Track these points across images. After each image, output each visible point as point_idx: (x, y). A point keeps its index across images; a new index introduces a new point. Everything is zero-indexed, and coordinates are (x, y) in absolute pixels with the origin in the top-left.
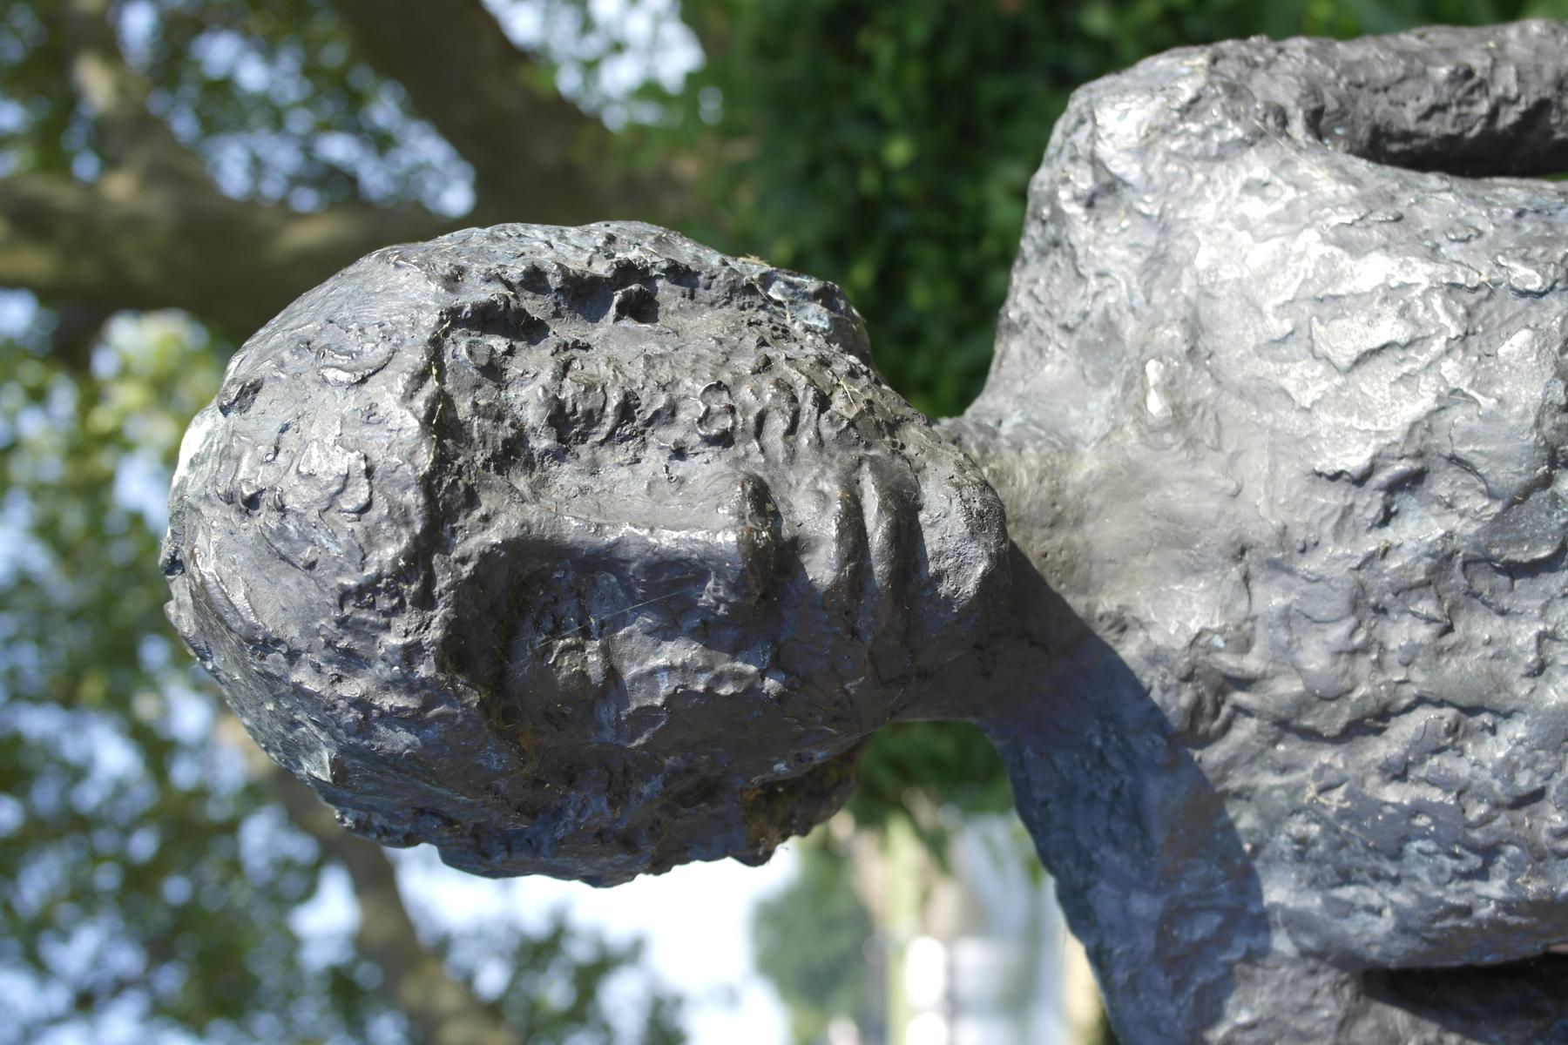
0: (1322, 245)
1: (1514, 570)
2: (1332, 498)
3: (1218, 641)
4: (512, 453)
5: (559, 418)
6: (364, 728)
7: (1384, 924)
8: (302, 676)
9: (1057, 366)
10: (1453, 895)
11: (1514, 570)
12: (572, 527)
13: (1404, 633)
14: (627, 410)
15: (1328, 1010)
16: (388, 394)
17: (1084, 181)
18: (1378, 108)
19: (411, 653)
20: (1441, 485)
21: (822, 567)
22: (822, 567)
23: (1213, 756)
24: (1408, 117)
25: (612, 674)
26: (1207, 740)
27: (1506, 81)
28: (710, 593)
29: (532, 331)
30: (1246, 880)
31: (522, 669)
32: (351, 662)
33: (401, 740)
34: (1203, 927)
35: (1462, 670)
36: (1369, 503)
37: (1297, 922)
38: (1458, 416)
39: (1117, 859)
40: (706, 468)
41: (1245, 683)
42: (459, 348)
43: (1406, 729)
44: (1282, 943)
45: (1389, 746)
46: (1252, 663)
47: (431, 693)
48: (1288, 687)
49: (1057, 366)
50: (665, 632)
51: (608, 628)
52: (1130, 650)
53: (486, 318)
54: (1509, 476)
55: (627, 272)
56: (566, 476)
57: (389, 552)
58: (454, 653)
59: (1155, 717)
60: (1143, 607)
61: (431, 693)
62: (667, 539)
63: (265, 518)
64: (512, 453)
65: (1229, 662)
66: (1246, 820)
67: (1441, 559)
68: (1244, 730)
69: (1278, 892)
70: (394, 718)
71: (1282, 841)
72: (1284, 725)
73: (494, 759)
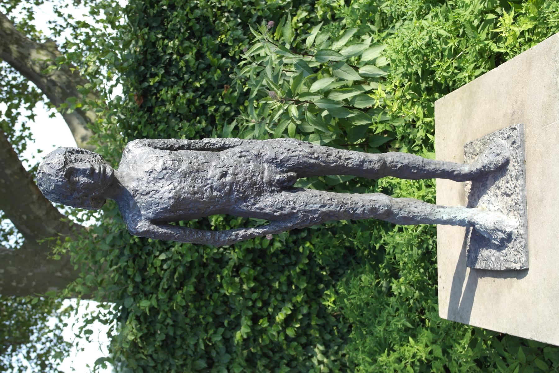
0: (33, 24)
5: (75, 159)
6: (57, 182)
7: (151, 214)
9: (124, 166)
10: (156, 209)
12: (76, 167)
13: (152, 185)
14: (81, 159)
17: (127, 150)
20: (154, 172)
21: (97, 171)
22: (97, 171)
23: (135, 198)
24: (159, 146)
25: (79, 180)
26: (135, 197)
28: (87, 172)
29: (73, 154)
30: (139, 211)
31: (71, 179)
32: (57, 176)
33: (60, 183)
34: (136, 217)
35: (155, 188)
36: (148, 174)
38: (156, 166)
40: (88, 164)
41: (138, 190)
42: (67, 153)
43: (151, 193)
44: (143, 218)
45: (150, 195)
46: (138, 189)
47: (64, 179)
48: (141, 190)
49: (124, 166)
50: (83, 177)
51: (78, 176)
52: (128, 189)
53: (69, 152)
54: (159, 171)
55: (81, 151)
56: (76, 164)
57: (61, 167)
58: (66, 175)
59: (130, 195)
60: (129, 185)
61: (64, 179)
62: (84, 167)
63: (50, 165)
64: (71, 161)
65: (136, 189)
66: (139, 205)
67: (154, 178)
69: (143, 212)
70: (60, 181)
71: (142, 207)
72: (142, 194)
73: (68, 186)
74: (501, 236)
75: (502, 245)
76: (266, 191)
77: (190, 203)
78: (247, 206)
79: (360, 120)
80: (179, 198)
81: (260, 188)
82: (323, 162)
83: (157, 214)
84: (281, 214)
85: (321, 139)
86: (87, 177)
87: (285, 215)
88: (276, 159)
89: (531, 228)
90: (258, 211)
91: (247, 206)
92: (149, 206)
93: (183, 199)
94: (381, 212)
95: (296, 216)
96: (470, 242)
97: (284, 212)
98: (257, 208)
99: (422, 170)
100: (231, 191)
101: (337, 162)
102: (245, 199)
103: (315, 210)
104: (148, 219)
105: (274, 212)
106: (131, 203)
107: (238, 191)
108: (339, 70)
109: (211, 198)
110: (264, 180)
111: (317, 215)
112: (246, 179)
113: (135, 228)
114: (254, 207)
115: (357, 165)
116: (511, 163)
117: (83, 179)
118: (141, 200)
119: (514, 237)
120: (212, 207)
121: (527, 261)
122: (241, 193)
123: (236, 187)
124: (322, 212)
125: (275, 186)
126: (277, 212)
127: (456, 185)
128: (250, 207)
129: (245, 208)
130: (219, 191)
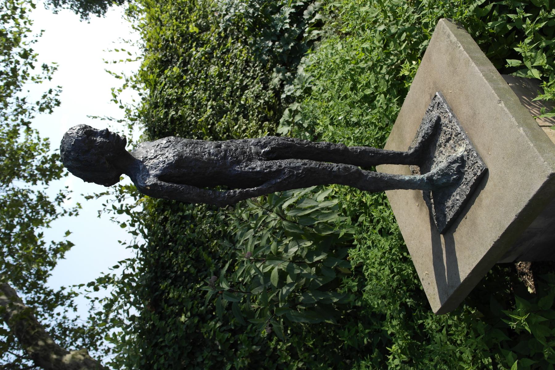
30: (148, 172)
69: (151, 172)
74: (456, 166)
75: (460, 173)
76: (255, 158)
77: (191, 162)
78: (241, 168)
79: (326, 232)
80: (182, 156)
81: (249, 156)
82: (298, 144)
83: (164, 170)
84: (270, 171)
85: (298, 244)
86: (103, 138)
87: (274, 172)
88: (260, 142)
89: (476, 141)
90: (251, 170)
91: (241, 168)
92: (155, 167)
93: (186, 157)
94: (353, 170)
95: (283, 172)
96: (435, 212)
97: (273, 170)
98: (249, 168)
99: (377, 153)
100: (225, 156)
101: (308, 144)
102: (239, 162)
103: (298, 167)
104: (154, 176)
105: (264, 169)
106: (141, 167)
107: (232, 156)
108: (302, 204)
109: (209, 160)
110: (252, 151)
111: (300, 171)
112: (237, 149)
113: (144, 183)
114: (246, 169)
115: (325, 146)
116: (442, 118)
117: (99, 139)
118: (149, 164)
119: (465, 159)
120: (211, 168)
121: (484, 164)
122: (235, 158)
123: (230, 153)
124: (305, 168)
125: (262, 156)
126: (266, 169)
127: (410, 193)
128: (243, 168)
129: (239, 169)
130: (216, 155)
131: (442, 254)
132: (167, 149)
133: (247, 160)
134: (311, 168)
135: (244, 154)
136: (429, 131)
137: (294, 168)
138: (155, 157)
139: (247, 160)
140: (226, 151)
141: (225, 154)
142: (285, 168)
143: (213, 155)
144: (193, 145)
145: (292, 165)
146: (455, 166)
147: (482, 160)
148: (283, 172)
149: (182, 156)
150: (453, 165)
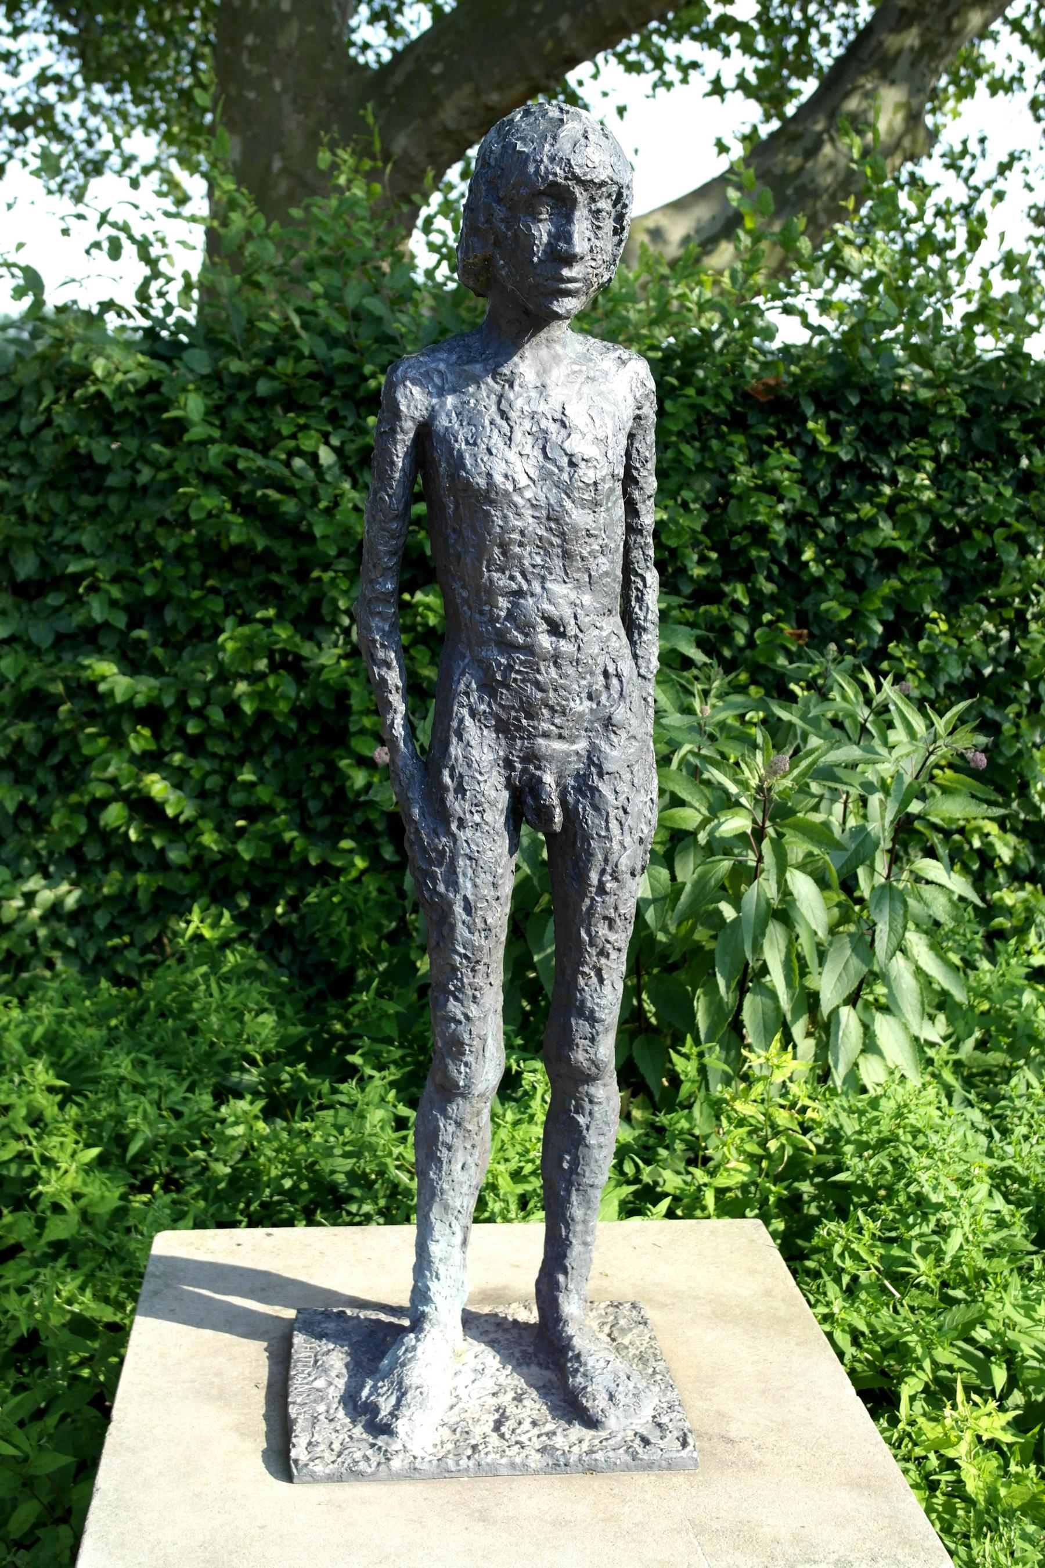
1: (544, 449)
2: (559, 408)
3: (870, 136)
4: (593, 200)
5: (599, 211)
8: (547, 147)
9: (580, 349)
10: (460, 437)
11: (544, 449)
12: (577, 214)
13: (527, 425)
15: (417, 414)
16: (609, 172)
18: (639, 437)
19: (555, 174)
20: (564, 432)
21: (566, 272)
23: (489, 380)
24: (637, 445)
26: (494, 379)
27: (644, 473)
29: (614, 206)
30: (454, 391)
31: (544, 199)
32: (552, 159)
34: (437, 380)
35: (518, 436)
36: (558, 416)
37: (443, 405)
39: (454, 357)
40: (587, 246)
41: (511, 386)
42: (615, 188)
43: (504, 423)
44: (434, 401)
45: (499, 421)
46: (516, 388)
47: (545, 179)
49: (580, 349)
50: (549, 234)
52: (516, 359)
53: (620, 195)
54: (566, 445)
55: (623, 228)
56: (586, 212)
57: (578, 171)
58: (555, 184)
60: (527, 362)
61: (545, 179)
63: (583, 141)
64: (593, 200)
66: (471, 389)
68: (497, 388)
69: (450, 400)
70: (537, 168)
72: (501, 397)
73: (523, 191)
76: (511, 746)
77: (475, 532)
78: (467, 694)
79: (708, 1010)
80: (492, 502)
82: (591, 907)
83: (446, 440)
84: (446, 789)
85: (654, 901)
86: (549, 243)
87: (443, 801)
88: (601, 775)
89: (408, 1490)
90: (455, 724)
92: (469, 417)
93: (488, 514)
94: (452, 1067)
95: (440, 830)
97: (450, 796)
99: (570, 1183)
102: (489, 688)
104: (433, 414)
106: (478, 368)
107: (510, 668)
108: (848, 952)
109: (490, 592)
110: (541, 741)
111: (441, 888)
113: (405, 378)
114: (465, 712)
115: (583, 1001)
117: (542, 231)
120: (465, 594)
122: (505, 676)
123: (522, 663)
124: (450, 905)
125: (525, 771)
126: (452, 777)
128: (464, 700)
129: (462, 687)
130: (510, 616)
131: (261, 1300)
132: (537, 452)
133: (498, 719)
134: (453, 927)
135: (522, 709)
136: (579, 1379)
137: (452, 870)
138: (503, 415)
139: (498, 719)
140: (529, 649)
141: (518, 648)
142: (454, 838)
143: (515, 605)
144: (556, 541)
145: (462, 862)
146: (386, 1406)
147: (330, 1478)
148: (440, 830)
149: (492, 502)
150: (393, 1400)
